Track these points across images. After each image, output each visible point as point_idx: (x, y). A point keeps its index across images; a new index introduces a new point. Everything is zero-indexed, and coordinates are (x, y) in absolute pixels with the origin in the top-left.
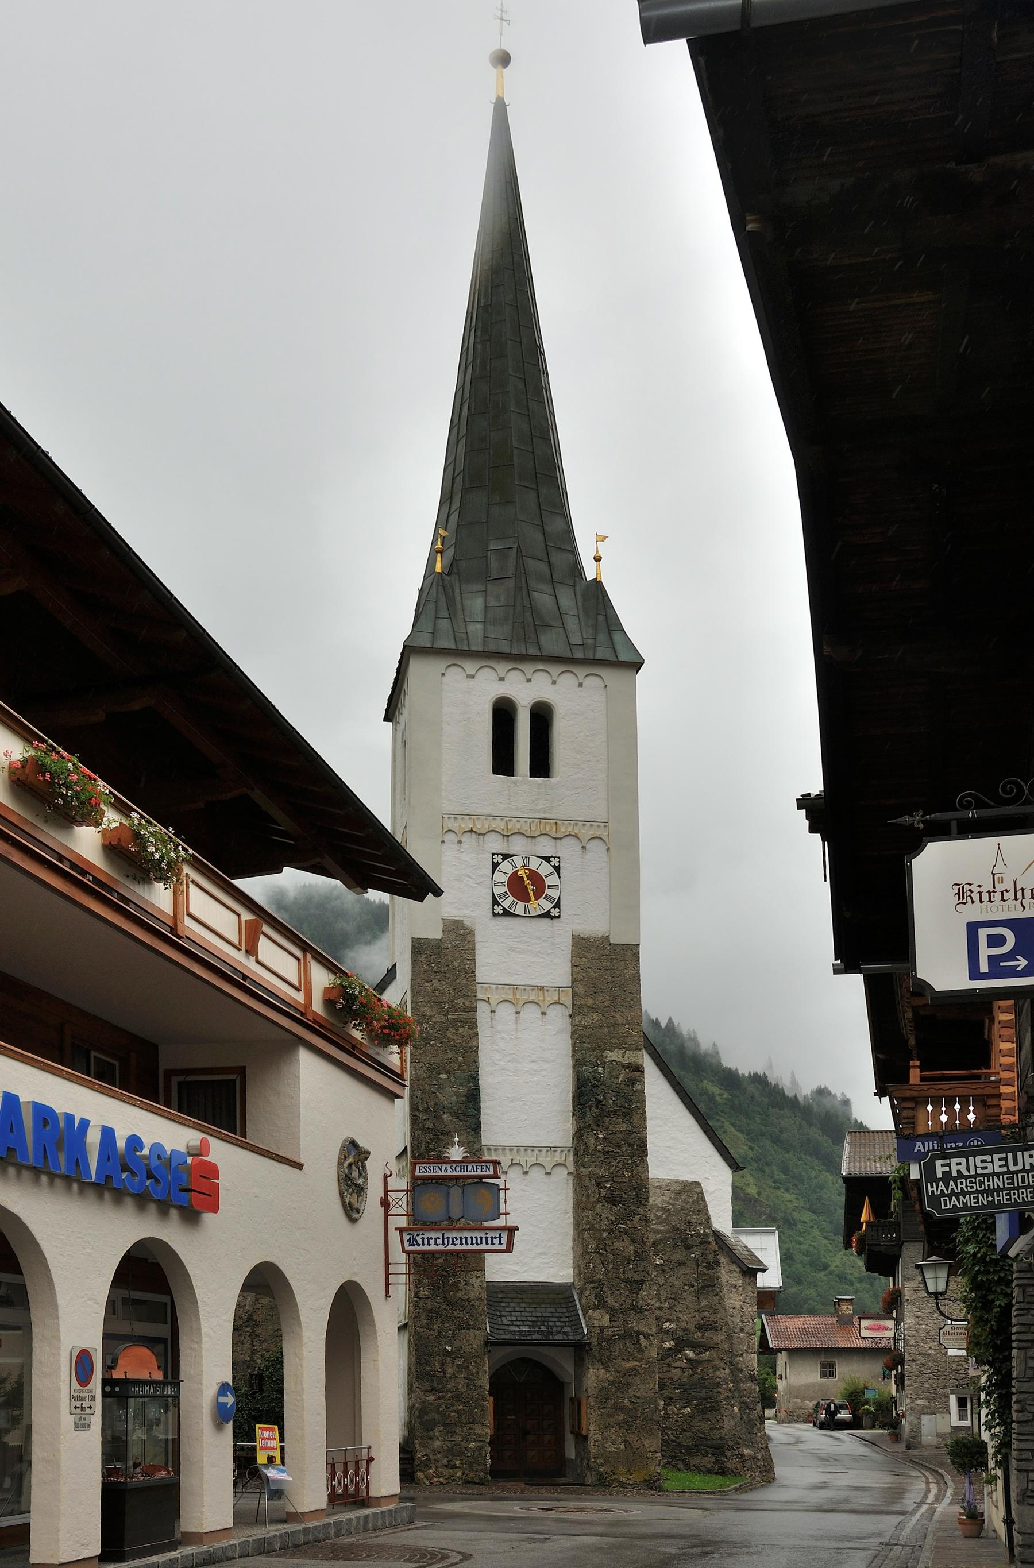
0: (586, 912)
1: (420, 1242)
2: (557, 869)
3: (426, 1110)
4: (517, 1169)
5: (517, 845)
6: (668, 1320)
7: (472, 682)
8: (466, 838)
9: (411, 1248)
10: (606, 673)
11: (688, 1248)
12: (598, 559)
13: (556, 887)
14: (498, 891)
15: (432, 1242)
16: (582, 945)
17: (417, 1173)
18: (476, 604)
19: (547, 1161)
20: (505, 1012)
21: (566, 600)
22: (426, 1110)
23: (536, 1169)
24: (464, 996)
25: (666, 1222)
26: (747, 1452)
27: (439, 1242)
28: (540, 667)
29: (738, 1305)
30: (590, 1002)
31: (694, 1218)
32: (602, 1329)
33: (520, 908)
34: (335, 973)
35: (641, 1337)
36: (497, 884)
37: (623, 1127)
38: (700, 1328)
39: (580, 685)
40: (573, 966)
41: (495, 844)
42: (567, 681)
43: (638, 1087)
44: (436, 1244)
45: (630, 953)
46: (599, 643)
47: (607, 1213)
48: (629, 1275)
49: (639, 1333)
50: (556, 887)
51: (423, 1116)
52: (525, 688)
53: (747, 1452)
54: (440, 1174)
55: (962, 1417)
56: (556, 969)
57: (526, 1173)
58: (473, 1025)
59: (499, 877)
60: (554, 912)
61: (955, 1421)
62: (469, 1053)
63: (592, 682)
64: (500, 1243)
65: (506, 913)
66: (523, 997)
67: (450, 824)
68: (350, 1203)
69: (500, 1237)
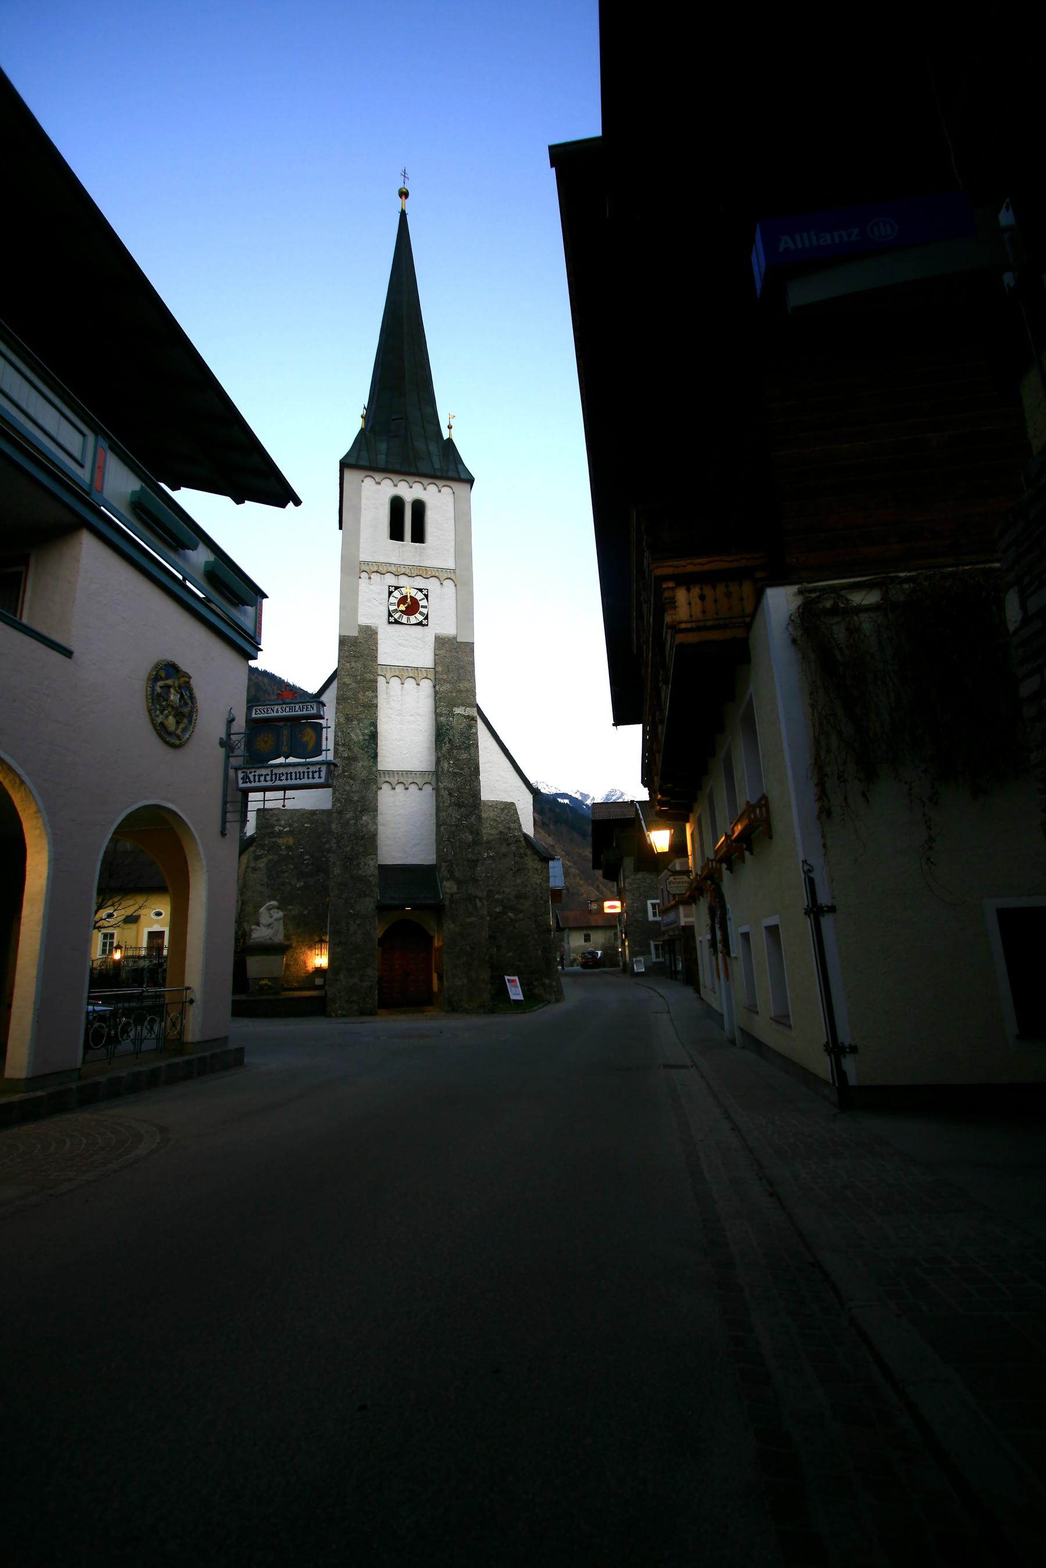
0: (443, 620)
1: (252, 779)
2: (426, 596)
3: (343, 745)
4: (401, 786)
5: (403, 581)
6: (498, 893)
7: (378, 486)
8: (373, 576)
9: (245, 785)
10: (454, 485)
11: (508, 845)
12: (450, 427)
13: (425, 607)
14: (392, 608)
15: (262, 778)
16: (441, 642)
17: (254, 716)
18: (383, 446)
19: (419, 781)
20: (395, 682)
21: (433, 448)
22: (343, 745)
23: (413, 786)
24: (370, 672)
25: (496, 828)
26: (547, 981)
27: (268, 778)
28: (417, 479)
29: (539, 882)
30: (445, 677)
31: (512, 826)
32: (452, 895)
33: (404, 620)
34: (143, 480)
35: (477, 901)
36: (392, 604)
37: (465, 756)
38: (517, 897)
39: (440, 491)
40: (435, 655)
41: (391, 580)
42: (432, 488)
43: (473, 731)
44: (266, 781)
45: (469, 647)
46: (448, 467)
47: (455, 814)
48: (470, 856)
49: (476, 897)
50: (425, 607)
51: (341, 749)
52: (410, 491)
53: (547, 981)
54: (272, 714)
55: (657, 956)
56: (425, 658)
57: (407, 789)
58: (375, 690)
59: (392, 600)
60: (425, 622)
61: (654, 959)
62: (372, 707)
63: (446, 490)
64: (320, 777)
65: (397, 622)
66: (407, 673)
67: (364, 568)
68: (162, 724)
69: (320, 771)
